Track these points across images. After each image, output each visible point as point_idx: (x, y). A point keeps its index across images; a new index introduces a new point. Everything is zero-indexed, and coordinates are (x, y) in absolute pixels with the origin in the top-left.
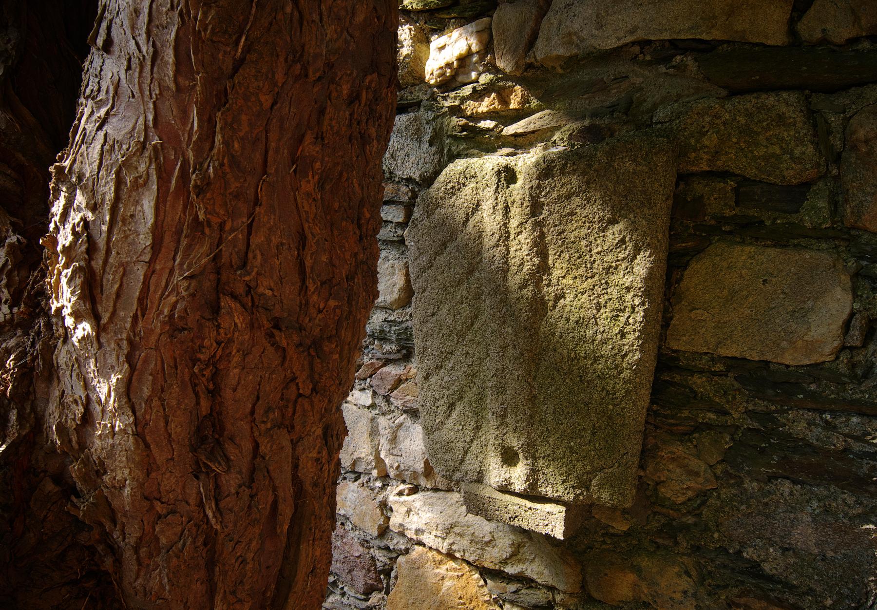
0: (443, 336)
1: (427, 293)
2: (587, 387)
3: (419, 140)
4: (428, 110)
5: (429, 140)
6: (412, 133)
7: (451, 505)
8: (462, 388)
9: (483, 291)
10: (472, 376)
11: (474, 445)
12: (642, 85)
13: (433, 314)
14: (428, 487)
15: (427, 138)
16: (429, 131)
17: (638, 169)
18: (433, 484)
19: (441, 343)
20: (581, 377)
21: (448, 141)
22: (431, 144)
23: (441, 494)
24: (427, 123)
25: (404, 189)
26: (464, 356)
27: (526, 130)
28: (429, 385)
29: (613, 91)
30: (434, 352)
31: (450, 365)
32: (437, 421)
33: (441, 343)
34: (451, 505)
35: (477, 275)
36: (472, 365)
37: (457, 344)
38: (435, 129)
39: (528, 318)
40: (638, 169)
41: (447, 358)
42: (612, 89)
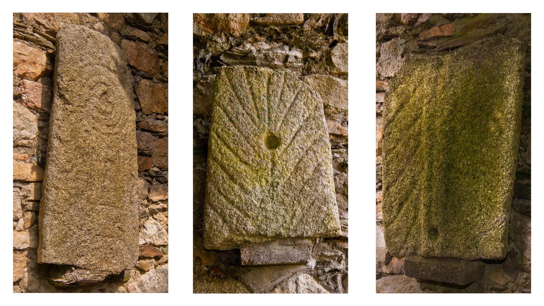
0: (398, 161)
1: (391, 136)
2: (477, 181)
3: (396, 55)
4: (402, 38)
5: (401, 54)
6: (392, 51)
7: (401, 283)
8: (407, 192)
9: (422, 130)
10: (414, 183)
11: (413, 229)
12: (512, 20)
13: (394, 148)
14: (387, 272)
15: (400, 53)
16: (401, 49)
17: (504, 54)
18: (391, 270)
19: (397, 165)
20: (473, 175)
21: (412, 55)
22: (402, 57)
23: (396, 276)
24: (401, 45)
25: (386, 83)
26: (410, 172)
27: (453, 46)
28: (388, 194)
29: (498, 23)
30: (393, 172)
31: (401, 179)
32: (392, 216)
33: (397, 165)
34: (401, 283)
35: (419, 121)
36: (414, 176)
37: (406, 164)
38: (405, 49)
39: (446, 142)
40: (504, 54)
41: (400, 174)
42: (497, 22)
